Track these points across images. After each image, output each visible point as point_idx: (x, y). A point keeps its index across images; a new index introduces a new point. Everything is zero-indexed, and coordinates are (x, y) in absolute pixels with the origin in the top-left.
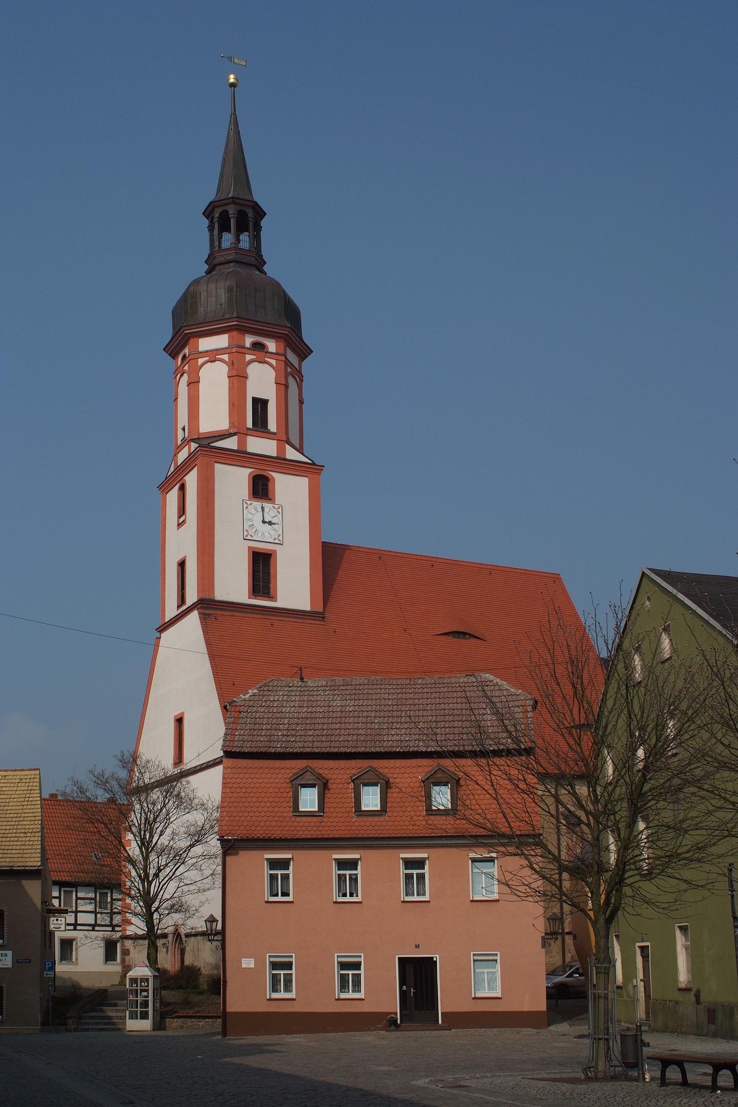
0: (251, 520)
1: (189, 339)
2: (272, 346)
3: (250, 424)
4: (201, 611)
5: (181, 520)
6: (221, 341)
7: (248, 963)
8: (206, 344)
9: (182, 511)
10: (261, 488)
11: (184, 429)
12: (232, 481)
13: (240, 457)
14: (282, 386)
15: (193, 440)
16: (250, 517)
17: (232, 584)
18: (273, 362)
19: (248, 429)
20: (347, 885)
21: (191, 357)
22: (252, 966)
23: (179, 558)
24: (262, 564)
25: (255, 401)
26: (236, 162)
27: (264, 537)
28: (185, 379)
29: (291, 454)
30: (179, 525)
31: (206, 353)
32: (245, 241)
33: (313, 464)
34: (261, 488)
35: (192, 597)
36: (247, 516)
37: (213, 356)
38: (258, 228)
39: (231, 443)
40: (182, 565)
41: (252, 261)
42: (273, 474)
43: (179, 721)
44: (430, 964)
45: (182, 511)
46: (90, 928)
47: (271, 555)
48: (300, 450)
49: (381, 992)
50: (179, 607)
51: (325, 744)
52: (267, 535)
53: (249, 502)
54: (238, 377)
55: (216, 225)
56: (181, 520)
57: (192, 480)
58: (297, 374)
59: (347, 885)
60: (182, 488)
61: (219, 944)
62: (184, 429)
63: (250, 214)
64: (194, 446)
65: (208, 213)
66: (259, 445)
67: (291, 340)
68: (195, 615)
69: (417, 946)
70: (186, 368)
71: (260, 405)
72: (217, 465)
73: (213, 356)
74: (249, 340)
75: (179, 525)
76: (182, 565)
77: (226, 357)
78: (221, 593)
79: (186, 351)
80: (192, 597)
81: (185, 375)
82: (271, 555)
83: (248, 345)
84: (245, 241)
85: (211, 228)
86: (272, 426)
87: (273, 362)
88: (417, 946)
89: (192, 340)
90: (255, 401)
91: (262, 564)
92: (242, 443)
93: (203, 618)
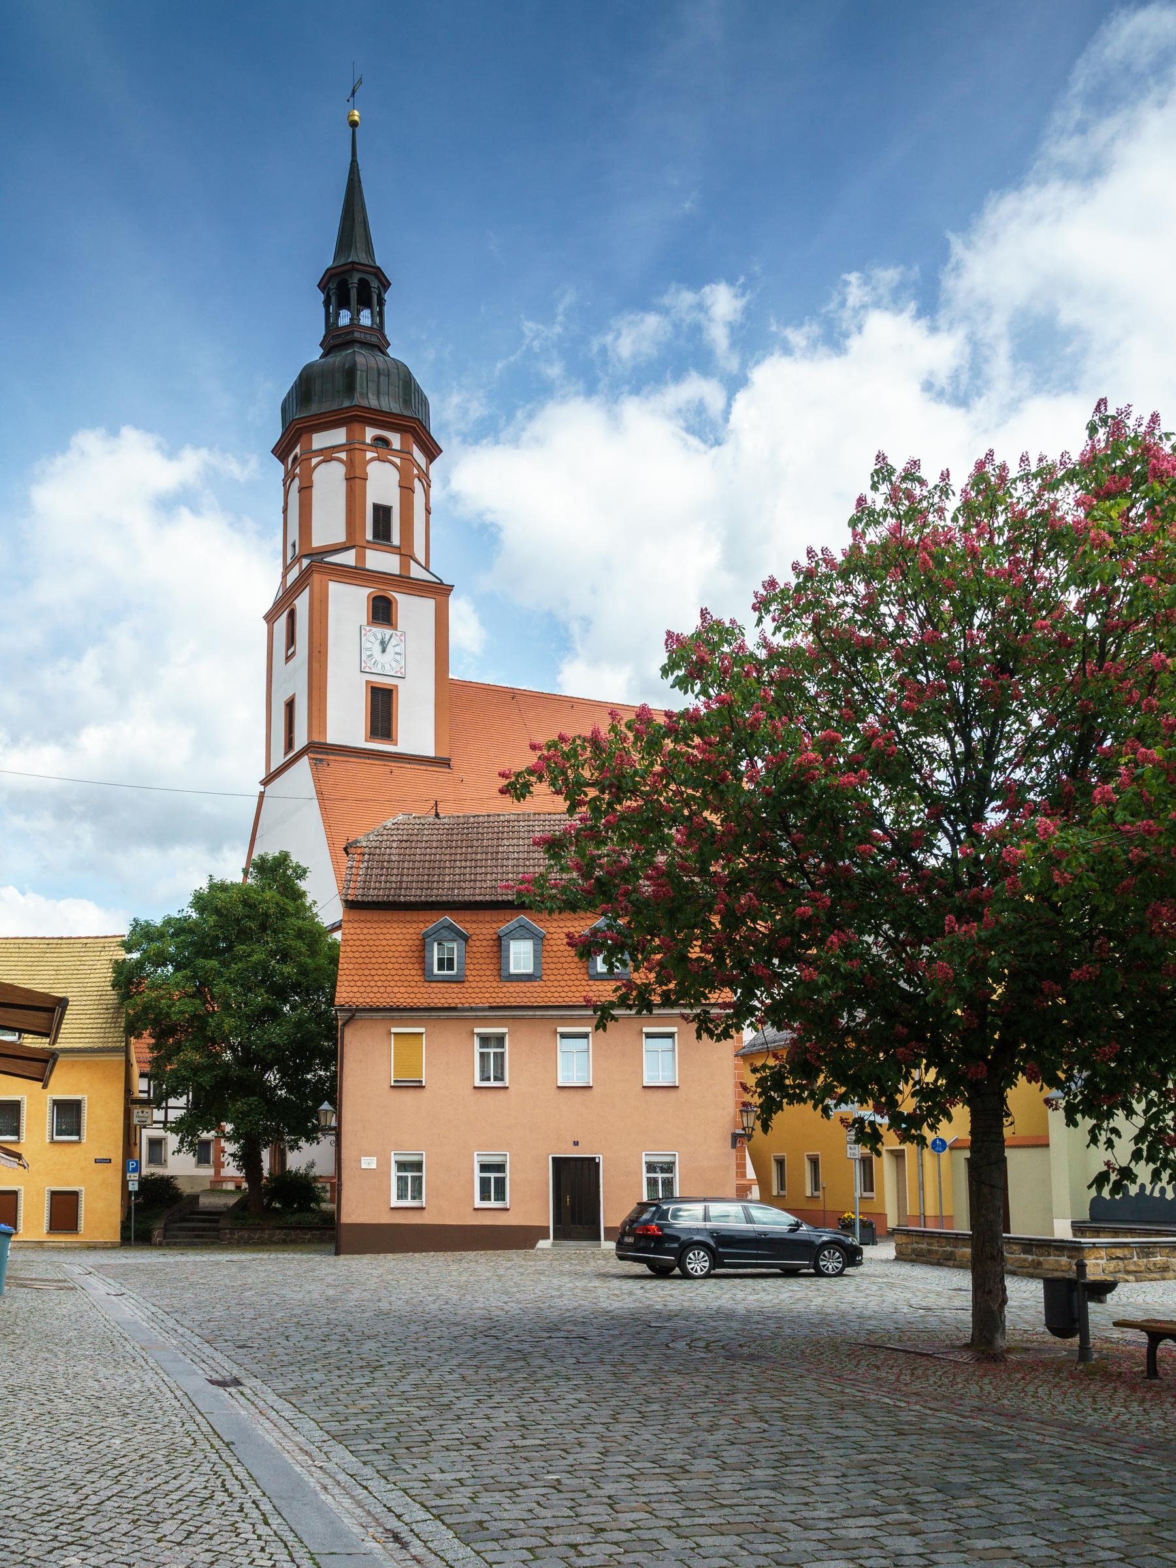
0: (370, 649)
1: (300, 436)
2: (396, 440)
3: (369, 536)
4: (312, 755)
5: (290, 652)
6: (338, 436)
7: (369, 1163)
8: (321, 440)
9: (291, 640)
10: (382, 612)
11: (294, 545)
12: (348, 604)
13: (357, 575)
14: (406, 489)
15: (305, 556)
16: (369, 645)
17: (347, 723)
18: (398, 461)
19: (368, 542)
20: (493, 1068)
21: (304, 457)
22: (374, 1166)
23: (287, 697)
24: (382, 706)
25: (377, 508)
26: (353, 223)
27: (385, 667)
28: (296, 483)
29: (416, 572)
30: (288, 658)
31: (321, 451)
32: (365, 318)
33: (442, 583)
34: (382, 612)
35: (301, 740)
36: (366, 644)
37: (328, 454)
38: (381, 302)
39: (348, 558)
40: (290, 705)
41: (374, 340)
42: (398, 596)
43: (96, 1161)
44: (590, 1166)
45: (291, 640)
46: (161, 1125)
47: (391, 691)
48: (427, 569)
49: (531, 1201)
50: (286, 754)
51: (467, 892)
52: (387, 667)
53: (368, 628)
54: (355, 481)
55: (333, 299)
56: (290, 652)
57: (302, 604)
58: (425, 477)
59: (493, 1068)
60: (292, 616)
61: (333, 1138)
62: (294, 545)
63: (374, 284)
64: (305, 562)
65: (323, 286)
66: (382, 561)
67: (204, 1221)
68: (305, 760)
69: (576, 1144)
70: (297, 471)
71: (382, 513)
72: (331, 583)
73: (328, 454)
74: (370, 433)
75: (288, 658)
76: (290, 705)
77: (343, 455)
78: (333, 737)
79: (298, 450)
80: (301, 740)
81: (297, 481)
82: (391, 691)
83: (368, 441)
84: (365, 318)
85: (327, 303)
86: (396, 540)
87: (398, 461)
88: (576, 1144)
89: (304, 438)
90: (377, 508)
91: (382, 706)
92: (361, 557)
93: (315, 763)
